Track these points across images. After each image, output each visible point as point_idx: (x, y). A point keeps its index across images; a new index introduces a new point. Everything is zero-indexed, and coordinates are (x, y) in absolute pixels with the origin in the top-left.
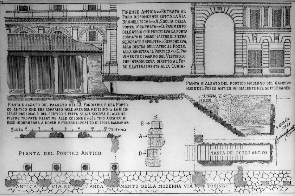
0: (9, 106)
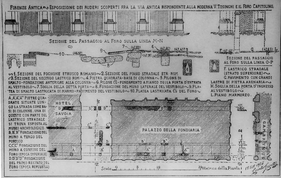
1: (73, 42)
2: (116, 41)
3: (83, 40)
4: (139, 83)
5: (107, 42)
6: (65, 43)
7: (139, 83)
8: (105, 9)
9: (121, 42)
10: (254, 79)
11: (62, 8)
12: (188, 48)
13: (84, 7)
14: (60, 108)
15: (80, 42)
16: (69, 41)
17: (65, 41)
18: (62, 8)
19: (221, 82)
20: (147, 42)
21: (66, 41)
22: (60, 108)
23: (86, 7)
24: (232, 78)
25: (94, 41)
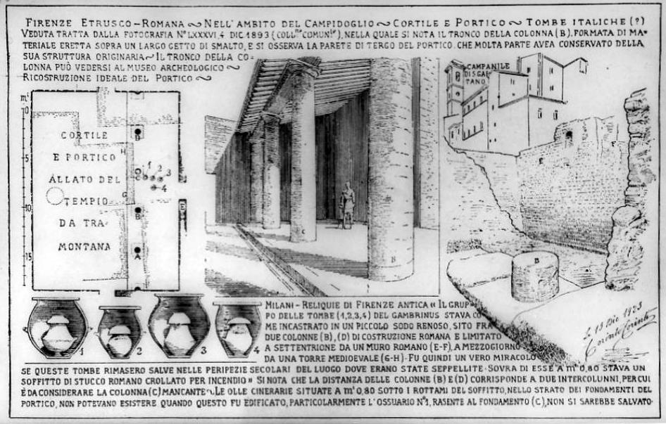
0: (191, 383)
4: (482, 403)
7: (482, 403)
24: (539, 46)
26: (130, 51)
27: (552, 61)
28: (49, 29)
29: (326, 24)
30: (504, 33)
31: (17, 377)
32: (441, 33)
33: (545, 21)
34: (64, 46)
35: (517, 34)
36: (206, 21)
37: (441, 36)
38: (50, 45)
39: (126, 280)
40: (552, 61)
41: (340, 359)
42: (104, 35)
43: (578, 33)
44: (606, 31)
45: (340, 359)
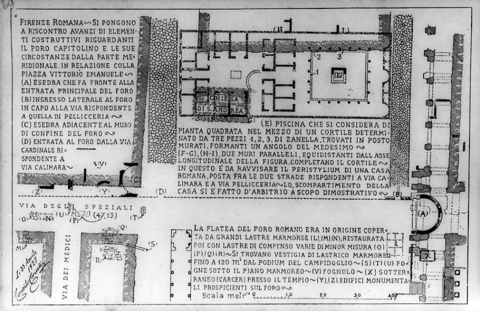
1: (359, 232)
2: (50, 124)
3: (71, 21)
5: (81, 58)
6: (359, 232)
8: (366, 233)
9: (332, 163)
10: (369, 233)
11: (350, 232)
12: (175, 262)
13: (274, 229)
14: (46, 206)
15: (22, 23)
16: (323, 192)
17: (254, 130)
18: (350, 232)
19: (265, 228)
20: (44, 21)
21: (304, 177)
22: (46, 206)
23: (277, 229)
25: (95, 39)
26: (377, 251)
27: (308, 117)
28: (270, 165)
29: (313, 185)
30: (48, 116)
31: (421, 302)
32: (23, 47)
33: (338, 184)
34: (37, 142)
35: (261, 246)
36: (249, 130)
37: (23, 49)
38: (50, 150)
39: (277, 64)
40: (308, 117)
41: (324, 148)
42: (49, 66)
43: (35, 49)
44: (236, 129)
45: (324, 148)
